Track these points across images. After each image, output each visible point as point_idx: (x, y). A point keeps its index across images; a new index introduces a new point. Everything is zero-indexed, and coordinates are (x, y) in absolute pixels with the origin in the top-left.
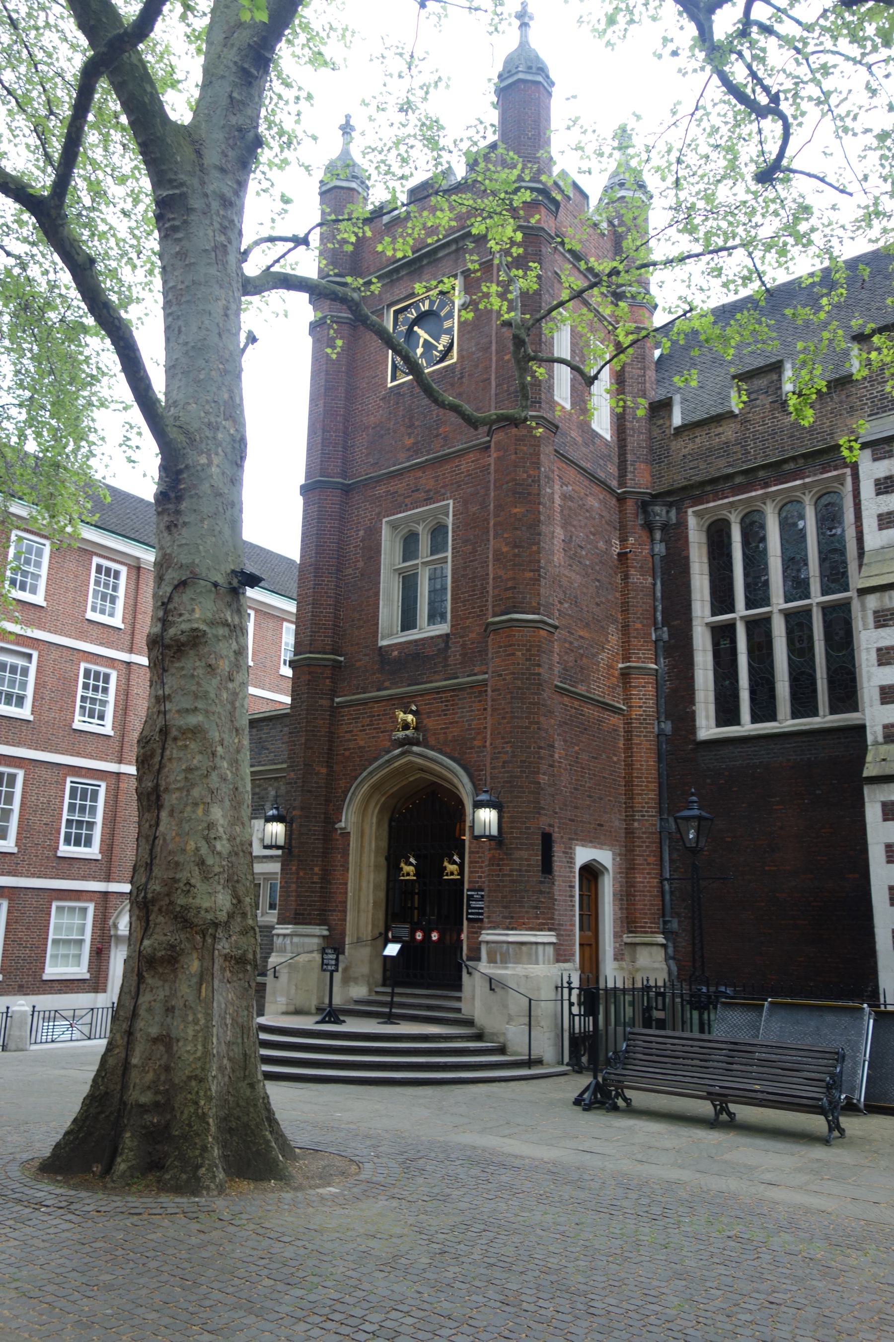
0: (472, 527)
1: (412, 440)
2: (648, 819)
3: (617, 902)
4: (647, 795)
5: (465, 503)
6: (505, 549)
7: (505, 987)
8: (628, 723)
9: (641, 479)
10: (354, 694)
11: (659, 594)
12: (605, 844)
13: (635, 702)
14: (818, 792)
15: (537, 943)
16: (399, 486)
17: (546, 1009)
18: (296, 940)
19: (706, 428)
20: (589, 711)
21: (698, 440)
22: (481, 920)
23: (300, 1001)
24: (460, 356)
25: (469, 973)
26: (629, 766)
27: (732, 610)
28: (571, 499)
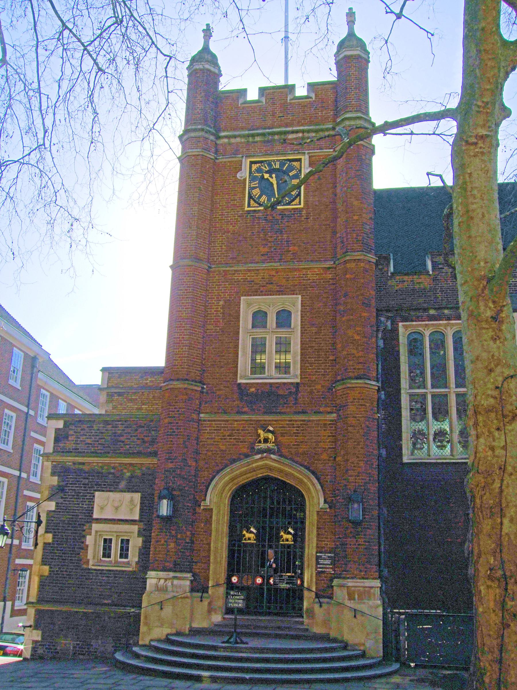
18: (176, 582)
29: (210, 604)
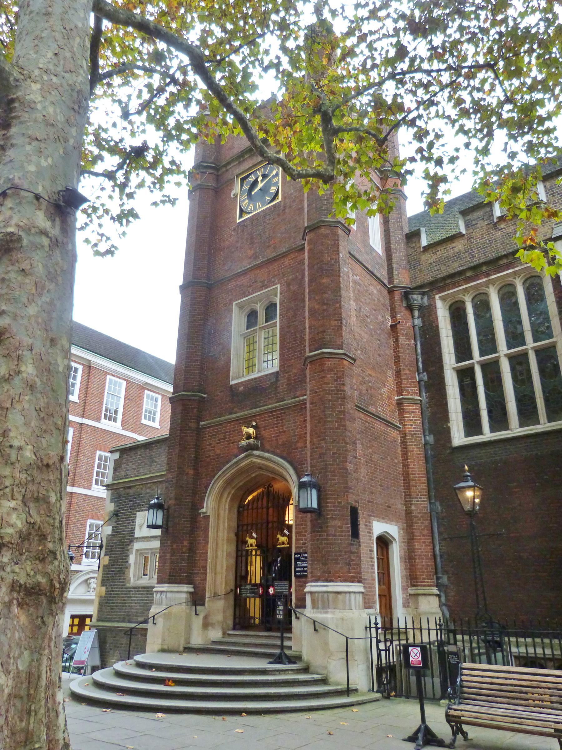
0: (294, 299)
1: (252, 252)
2: (421, 504)
3: (403, 564)
4: (420, 487)
5: (289, 285)
6: (317, 307)
7: (325, 627)
8: (404, 436)
9: (403, 279)
10: (213, 419)
11: (419, 351)
12: (393, 521)
13: (407, 422)
14: (545, 477)
15: (350, 593)
16: (244, 281)
17: (359, 645)
18: (169, 595)
19: (444, 245)
20: (379, 426)
21: (439, 253)
22: (306, 576)
23: (171, 643)
24: (284, 198)
25: (297, 618)
26: (406, 466)
27: (471, 358)
28: (359, 284)
29: (205, 618)
